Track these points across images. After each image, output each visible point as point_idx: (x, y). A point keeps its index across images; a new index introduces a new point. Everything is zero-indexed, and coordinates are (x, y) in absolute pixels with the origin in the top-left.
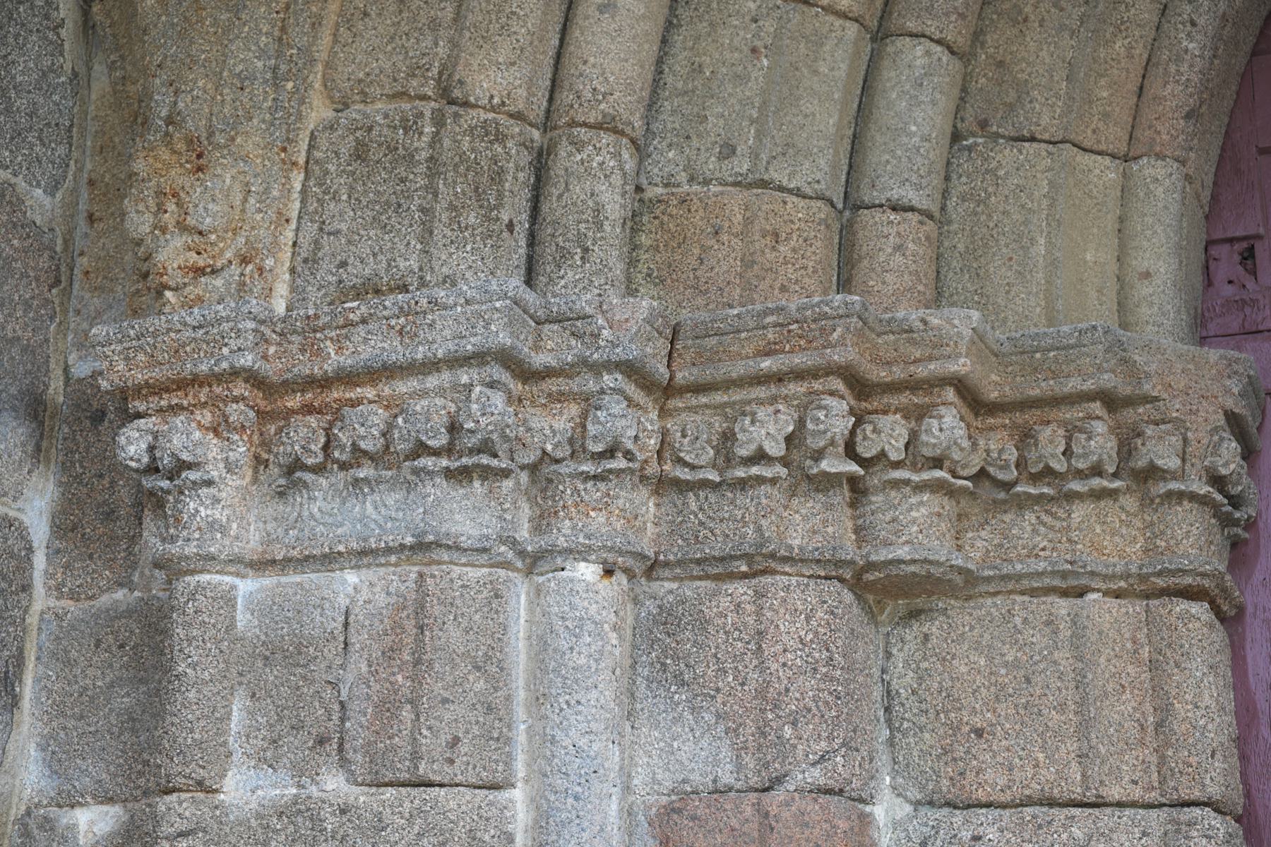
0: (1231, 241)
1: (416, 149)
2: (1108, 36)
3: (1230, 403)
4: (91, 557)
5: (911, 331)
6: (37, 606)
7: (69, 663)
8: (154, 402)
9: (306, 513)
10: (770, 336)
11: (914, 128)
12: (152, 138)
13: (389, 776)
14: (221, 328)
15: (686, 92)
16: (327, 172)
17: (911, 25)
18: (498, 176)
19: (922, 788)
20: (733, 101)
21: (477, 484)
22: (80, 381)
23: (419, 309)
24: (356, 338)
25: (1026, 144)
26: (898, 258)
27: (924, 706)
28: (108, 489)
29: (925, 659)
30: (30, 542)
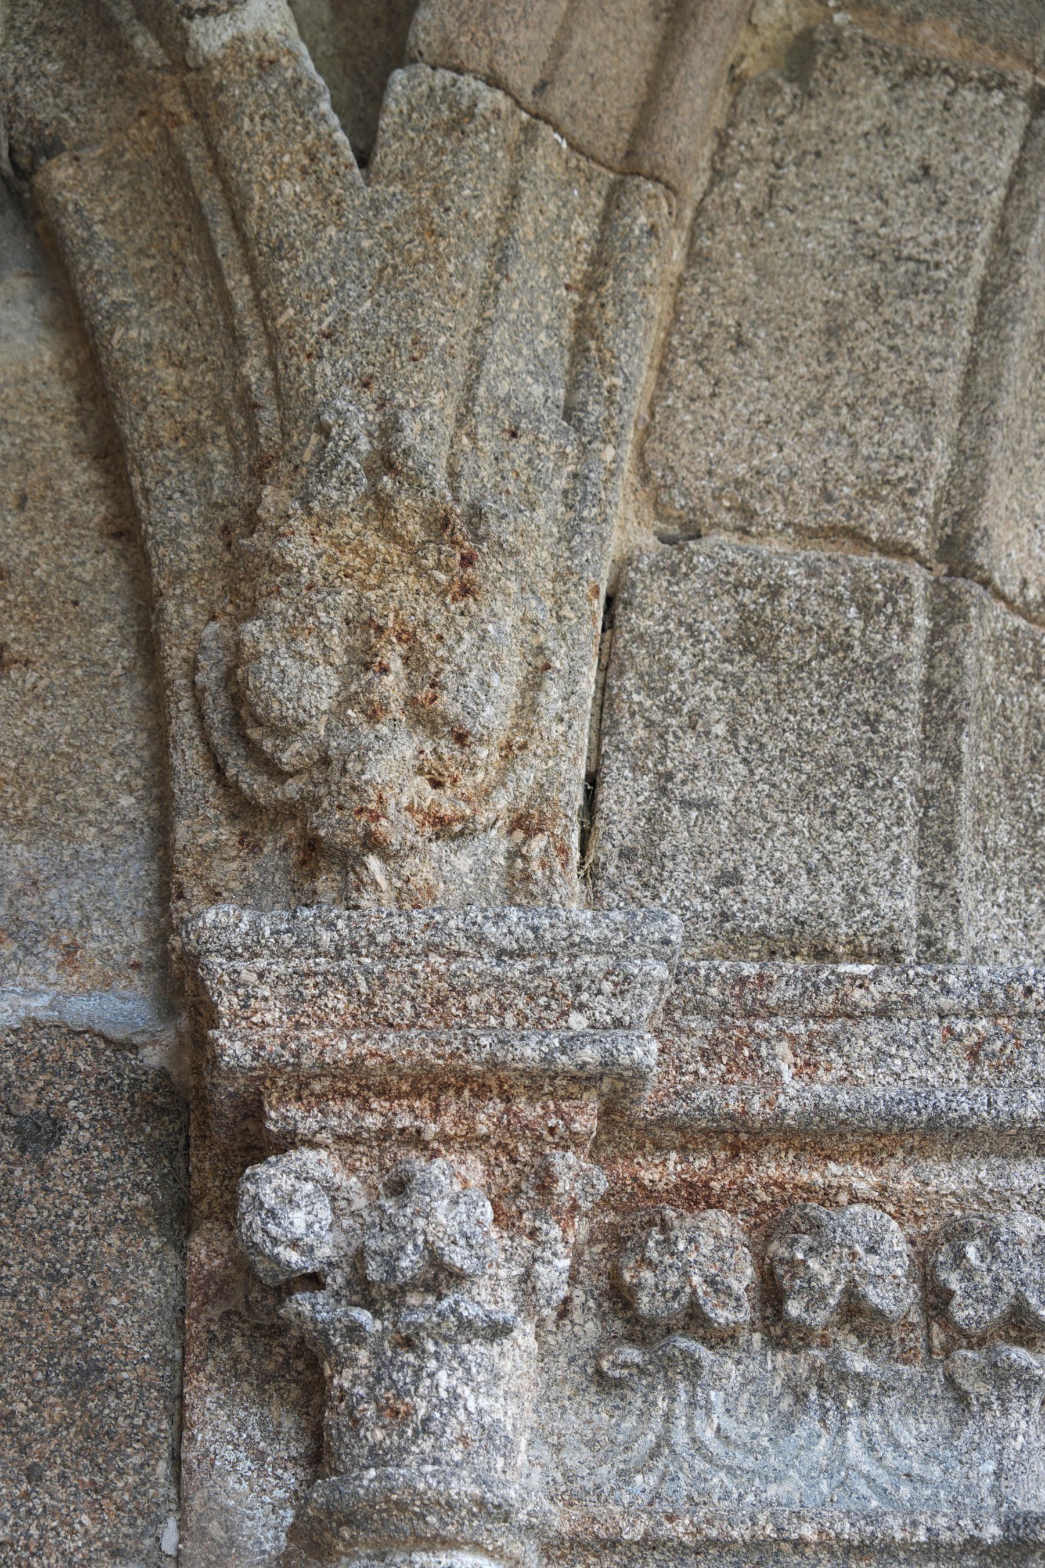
1: (898, 657)
9: (680, 1438)
12: (335, 495)
14: (578, 964)
23: (1031, 1006)
24: (859, 1049)
28: (79, 1312)
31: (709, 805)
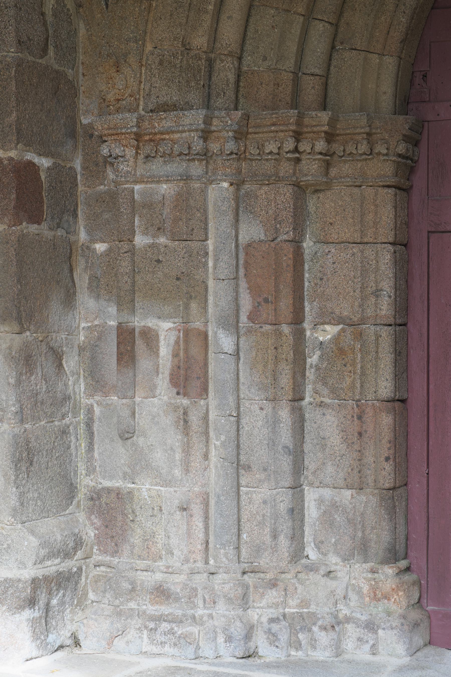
0: (421, 71)
2: (379, 16)
3: (404, 132)
4: (93, 176)
5: (313, 117)
6: (80, 190)
7: (90, 206)
8: (110, 138)
10: (274, 120)
11: (319, 50)
13: (177, 238)
15: (253, 38)
16: (152, 68)
17: (319, 17)
18: (200, 71)
19: (316, 238)
20: (266, 42)
21: (196, 162)
22: (85, 125)
25: (353, 51)
26: (313, 91)
27: (317, 216)
29: (318, 203)
30: (76, 172)
31: (156, 87)
